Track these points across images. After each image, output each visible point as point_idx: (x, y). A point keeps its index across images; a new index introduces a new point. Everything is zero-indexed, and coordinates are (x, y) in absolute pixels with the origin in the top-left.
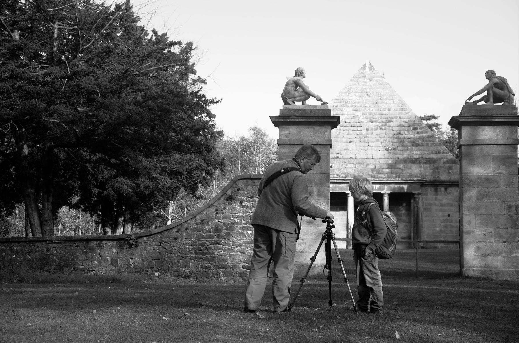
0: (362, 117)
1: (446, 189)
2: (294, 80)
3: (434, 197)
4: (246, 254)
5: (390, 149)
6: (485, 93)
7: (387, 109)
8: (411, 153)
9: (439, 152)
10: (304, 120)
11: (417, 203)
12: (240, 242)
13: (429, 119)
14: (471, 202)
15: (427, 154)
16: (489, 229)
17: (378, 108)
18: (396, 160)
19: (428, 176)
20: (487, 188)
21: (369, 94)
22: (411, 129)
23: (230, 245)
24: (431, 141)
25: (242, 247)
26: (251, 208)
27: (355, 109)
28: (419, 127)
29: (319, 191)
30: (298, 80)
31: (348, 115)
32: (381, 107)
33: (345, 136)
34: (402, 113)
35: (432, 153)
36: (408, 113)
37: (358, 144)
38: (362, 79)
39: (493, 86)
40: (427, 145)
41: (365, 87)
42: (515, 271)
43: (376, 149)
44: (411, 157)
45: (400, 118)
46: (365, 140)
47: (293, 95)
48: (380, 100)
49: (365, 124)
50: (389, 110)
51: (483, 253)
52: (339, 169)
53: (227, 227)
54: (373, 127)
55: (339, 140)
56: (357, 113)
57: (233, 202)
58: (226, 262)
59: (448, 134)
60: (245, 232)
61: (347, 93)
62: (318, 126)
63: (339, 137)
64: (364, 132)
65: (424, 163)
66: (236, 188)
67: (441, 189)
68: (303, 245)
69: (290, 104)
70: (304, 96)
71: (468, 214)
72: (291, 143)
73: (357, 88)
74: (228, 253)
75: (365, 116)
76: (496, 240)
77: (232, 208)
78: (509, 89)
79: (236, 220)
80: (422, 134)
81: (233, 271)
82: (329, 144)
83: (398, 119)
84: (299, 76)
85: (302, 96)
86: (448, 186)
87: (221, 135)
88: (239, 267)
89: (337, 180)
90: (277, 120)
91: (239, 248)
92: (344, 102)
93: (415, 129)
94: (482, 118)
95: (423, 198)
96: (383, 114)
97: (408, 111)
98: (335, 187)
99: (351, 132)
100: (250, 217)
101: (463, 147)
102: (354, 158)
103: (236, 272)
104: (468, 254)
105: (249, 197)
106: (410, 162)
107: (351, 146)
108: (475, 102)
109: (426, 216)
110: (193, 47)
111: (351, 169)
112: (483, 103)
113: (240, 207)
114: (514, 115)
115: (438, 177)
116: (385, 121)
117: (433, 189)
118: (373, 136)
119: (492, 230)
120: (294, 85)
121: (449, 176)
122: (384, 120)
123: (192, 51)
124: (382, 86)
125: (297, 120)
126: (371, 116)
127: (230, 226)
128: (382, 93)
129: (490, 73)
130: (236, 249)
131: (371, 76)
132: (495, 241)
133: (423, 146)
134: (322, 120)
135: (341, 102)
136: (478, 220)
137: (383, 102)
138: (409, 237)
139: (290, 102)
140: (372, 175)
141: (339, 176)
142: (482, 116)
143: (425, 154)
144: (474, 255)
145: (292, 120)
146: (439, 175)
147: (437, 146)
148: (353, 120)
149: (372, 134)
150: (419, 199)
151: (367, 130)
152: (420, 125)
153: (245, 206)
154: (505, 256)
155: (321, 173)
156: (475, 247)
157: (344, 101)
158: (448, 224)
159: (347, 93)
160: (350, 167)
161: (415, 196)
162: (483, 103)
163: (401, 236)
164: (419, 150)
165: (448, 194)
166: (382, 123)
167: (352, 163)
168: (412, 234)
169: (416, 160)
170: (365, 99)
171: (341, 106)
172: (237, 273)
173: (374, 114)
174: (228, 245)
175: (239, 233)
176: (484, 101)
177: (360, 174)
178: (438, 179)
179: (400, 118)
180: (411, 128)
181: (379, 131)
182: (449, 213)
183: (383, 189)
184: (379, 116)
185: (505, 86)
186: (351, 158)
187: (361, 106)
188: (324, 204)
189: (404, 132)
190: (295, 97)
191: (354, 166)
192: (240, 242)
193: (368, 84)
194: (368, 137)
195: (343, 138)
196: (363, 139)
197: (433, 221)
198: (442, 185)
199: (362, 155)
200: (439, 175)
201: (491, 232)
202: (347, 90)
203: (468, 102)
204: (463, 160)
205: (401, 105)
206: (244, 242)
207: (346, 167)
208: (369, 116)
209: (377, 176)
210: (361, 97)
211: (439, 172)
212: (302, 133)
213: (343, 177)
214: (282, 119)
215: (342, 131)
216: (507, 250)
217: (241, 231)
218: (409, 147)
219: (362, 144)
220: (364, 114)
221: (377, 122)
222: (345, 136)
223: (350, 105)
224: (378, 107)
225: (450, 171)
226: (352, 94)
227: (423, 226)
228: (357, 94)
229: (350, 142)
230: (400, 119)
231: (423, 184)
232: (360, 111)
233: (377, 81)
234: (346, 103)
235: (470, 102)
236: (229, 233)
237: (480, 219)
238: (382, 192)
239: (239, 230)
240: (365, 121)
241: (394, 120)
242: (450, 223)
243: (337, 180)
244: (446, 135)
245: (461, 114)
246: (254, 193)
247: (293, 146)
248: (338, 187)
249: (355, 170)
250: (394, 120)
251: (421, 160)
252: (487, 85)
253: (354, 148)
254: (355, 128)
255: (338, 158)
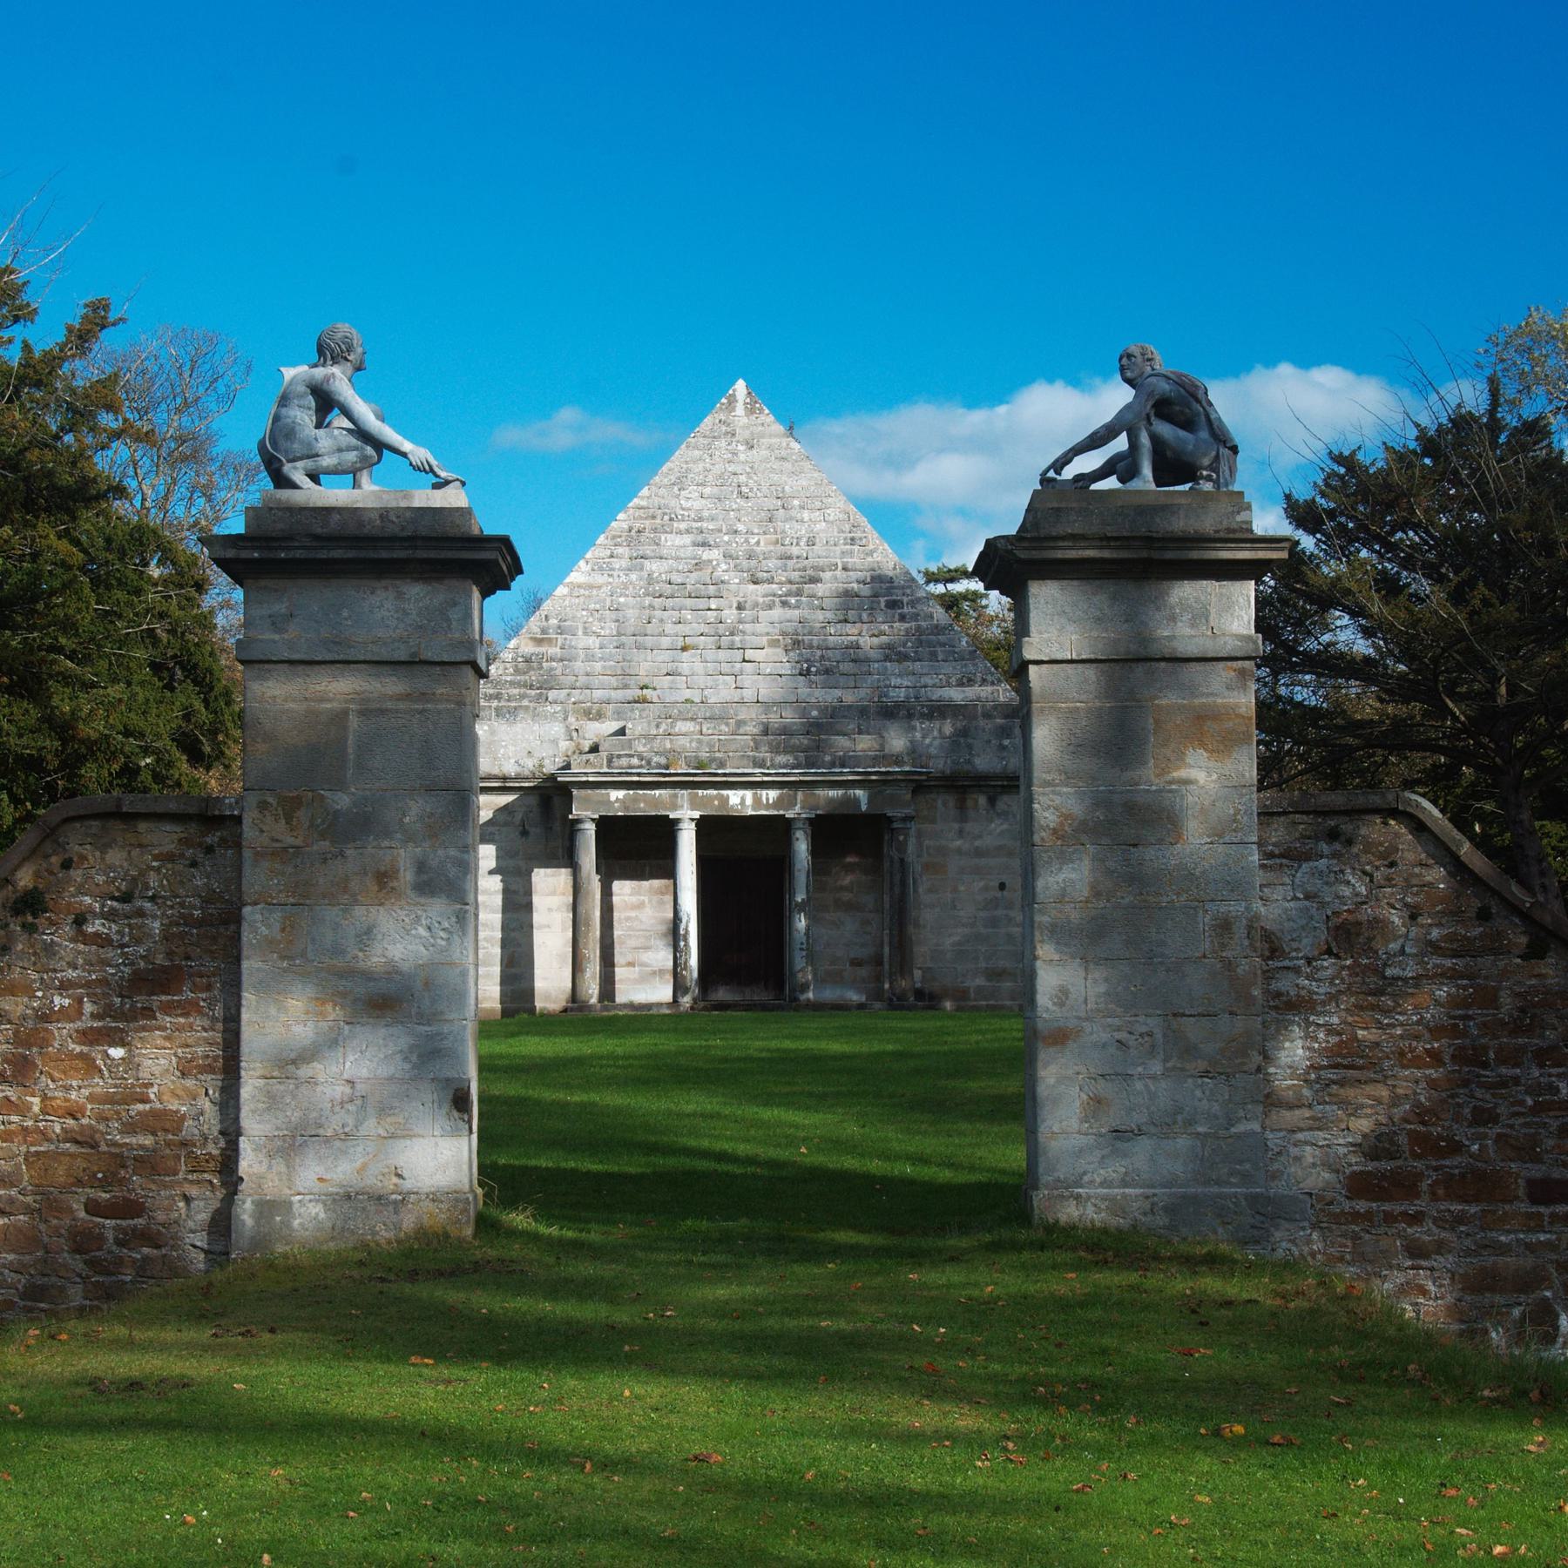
0: (724, 567)
1: (992, 801)
2: (312, 377)
3: (956, 826)
4: (104, 1148)
5: (813, 669)
6: (1121, 443)
7: (805, 539)
8: (882, 684)
9: (970, 680)
10: (351, 554)
11: (902, 848)
12: (73, 1095)
13: (952, 580)
14: (1068, 908)
15: (934, 686)
16: (1142, 1019)
17: (774, 537)
18: (835, 708)
19: (936, 757)
20: (1135, 845)
21: (745, 489)
22: (883, 605)
23: (29, 1109)
24: (944, 645)
25: (84, 1121)
26: (122, 946)
27: (700, 538)
28: (905, 599)
29: (421, 867)
30: (327, 379)
31: (677, 558)
32: (783, 532)
33: (669, 628)
34: (851, 553)
35: (949, 685)
36: (871, 553)
37: (711, 654)
38: (723, 443)
39: (1152, 414)
40: (933, 656)
41: (732, 468)
42: (1246, 1197)
43: (768, 671)
44: (880, 697)
45: (845, 569)
46: (733, 642)
47: (309, 445)
48: (781, 511)
49: (732, 587)
50: (811, 542)
51: (1115, 1124)
52: (649, 738)
53: (16, 1033)
54: (761, 600)
55: (649, 641)
56: (706, 555)
57: (41, 921)
58: (12, 1185)
59: (1003, 624)
60: (96, 1054)
61: (676, 488)
62: (417, 580)
63: (649, 632)
64: (730, 615)
65: (923, 716)
66: (54, 859)
67: (976, 801)
68: (351, 1107)
69: (295, 486)
70: (356, 448)
71: (1056, 957)
72: (296, 657)
73: (706, 470)
74: (23, 1148)
75: (732, 563)
76: (1169, 1065)
77: (38, 946)
78: (1216, 424)
79: (57, 1000)
80: (917, 620)
81: (42, 1227)
82: (465, 658)
83: (839, 573)
84: (335, 361)
85: (349, 449)
86: (999, 790)
87: (797, 643)
88: (70, 1210)
89: (639, 774)
90: (231, 554)
91: (71, 1122)
92: (666, 518)
93: (893, 605)
94: (1109, 547)
95: (919, 835)
96: (790, 558)
97: (871, 547)
98: (635, 800)
99: (688, 616)
100: (121, 986)
101: (1032, 669)
102: (697, 700)
103: (57, 1228)
104: (1055, 1129)
105: (113, 898)
106: (878, 713)
107: (688, 663)
108: (1079, 478)
109: (930, 891)
110: (112, 317)
111: (688, 739)
112: (1111, 483)
113: (72, 940)
114: (1238, 535)
115: (969, 762)
116: (798, 580)
117: (951, 800)
118: (760, 628)
119: (1154, 1024)
120: (311, 401)
121: (1003, 758)
122: (795, 576)
123: (104, 335)
124: (787, 466)
125: (323, 555)
126: (753, 563)
127: (30, 1024)
128: (787, 488)
129: (1139, 359)
130: (58, 1130)
131: (752, 433)
132: (1167, 1073)
133: (920, 660)
134: (432, 554)
135: (654, 517)
136: (1095, 981)
137: (791, 518)
138: (878, 961)
139: (299, 477)
140: (755, 757)
141: (649, 763)
142: (1109, 539)
143: (925, 687)
144: (1079, 1132)
145: (299, 554)
146: (970, 754)
147: (963, 659)
148: (694, 576)
149: (756, 620)
150: (906, 835)
151: (740, 607)
152: (908, 591)
153: (97, 935)
154: (1206, 1135)
155: (429, 790)
156: (1085, 1097)
157: (665, 514)
158: (1000, 912)
159: (676, 488)
160: (684, 730)
161: (895, 825)
162: (1111, 483)
163: (852, 955)
164: (908, 675)
165: (999, 815)
166: (789, 586)
167: (692, 719)
168: (887, 950)
169: (898, 705)
170: (734, 507)
171: (655, 530)
172: (60, 1236)
173: (761, 557)
174: (22, 1109)
175: (72, 1056)
176: (1114, 478)
177: (717, 755)
178: (967, 767)
179: (845, 569)
180: (882, 600)
181: (777, 613)
182: (1004, 878)
183: (792, 805)
184: (779, 563)
185: (1198, 414)
186: (687, 701)
187: (720, 531)
188: (446, 925)
189: (860, 616)
190: (317, 455)
191: (698, 728)
192: (73, 1095)
193: (742, 457)
194: (743, 632)
195: (663, 634)
196: (726, 638)
197: (954, 907)
198: (980, 786)
199: (724, 691)
200: (970, 754)
201: (1150, 1034)
202: (673, 478)
203: (1054, 480)
204: (1034, 726)
205: (847, 527)
206: (91, 1098)
207: (672, 731)
208: (745, 564)
209: (772, 760)
210: (719, 499)
211: (970, 747)
212: (345, 614)
213: (659, 766)
214: (254, 548)
215: (658, 613)
216: (1216, 1108)
217: (78, 1049)
218: (876, 665)
219: (722, 654)
220: (731, 557)
221: (771, 581)
222: (669, 628)
223: (683, 526)
224: (776, 532)
225: (1006, 742)
226: (692, 491)
227: (922, 922)
228: (707, 491)
229: (684, 649)
230: (845, 574)
231: (921, 785)
232: (717, 546)
233: (770, 448)
234: (671, 519)
235: (1058, 477)
236: (25, 1057)
237: (1106, 980)
238: (790, 814)
239: (71, 1046)
240: (734, 579)
241: (827, 575)
242: (1005, 912)
243: (639, 774)
244: (999, 626)
245: (1022, 528)
246: (134, 879)
247: (308, 669)
248: (645, 799)
249: (700, 742)
250: (827, 575)
251: (914, 708)
252: (1128, 407)
253: (699, 667)
254: (702, 603)
255: (645, 701)
